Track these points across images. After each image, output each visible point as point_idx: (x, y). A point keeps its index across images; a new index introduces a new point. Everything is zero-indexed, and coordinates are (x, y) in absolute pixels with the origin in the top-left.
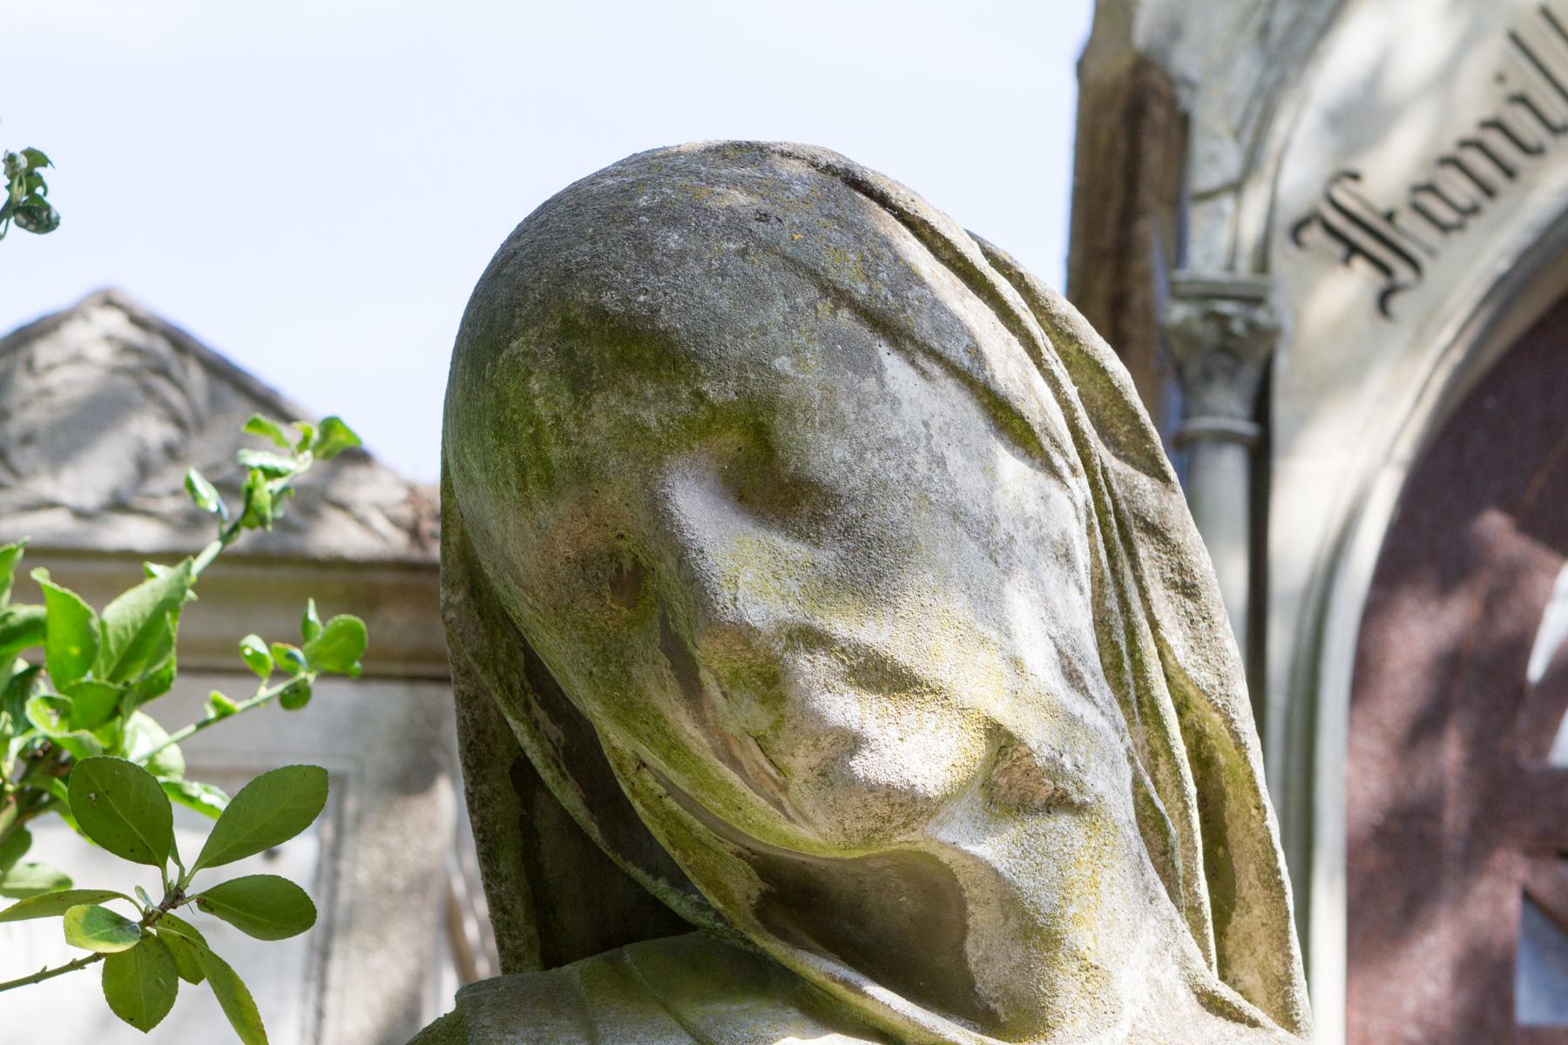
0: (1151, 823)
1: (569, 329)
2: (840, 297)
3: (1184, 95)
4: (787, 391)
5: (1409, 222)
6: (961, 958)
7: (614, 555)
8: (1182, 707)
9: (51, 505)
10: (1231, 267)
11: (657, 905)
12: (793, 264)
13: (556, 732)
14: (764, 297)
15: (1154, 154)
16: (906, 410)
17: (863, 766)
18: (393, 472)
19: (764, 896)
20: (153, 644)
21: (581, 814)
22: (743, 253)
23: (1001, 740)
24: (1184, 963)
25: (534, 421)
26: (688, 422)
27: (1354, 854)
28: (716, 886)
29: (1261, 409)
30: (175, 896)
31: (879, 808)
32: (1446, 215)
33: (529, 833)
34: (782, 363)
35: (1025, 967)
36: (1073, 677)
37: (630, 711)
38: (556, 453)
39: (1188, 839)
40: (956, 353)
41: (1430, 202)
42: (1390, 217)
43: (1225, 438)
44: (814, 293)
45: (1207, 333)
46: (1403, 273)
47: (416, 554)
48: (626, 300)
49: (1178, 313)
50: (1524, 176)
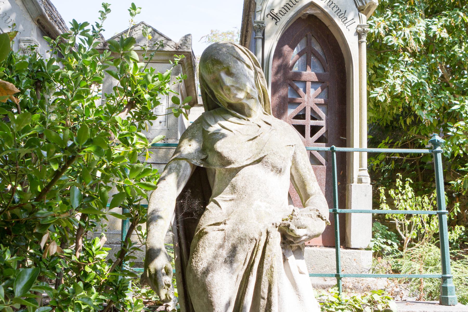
0: (259, 98)
1: (212, 60)
2: (234, 57)
5: (279, 14)
8: (262, 87)
9: (139, 45)
11: (217, 105)
12: (231, 54)
14: (228, 57)
15: (252, 6)
20: (168, 78)
21: (211, 98)
23: (248, 93)
29: (263, 35)
32: (283, 14)
33: (207, 99)
35: (250, 112)
36: (253, 87)
37: (217, 91)
38: (211, 71)
41: (281, 12)
42: (277, 14)
43: (260, 38)
45: (258, 27)
46: (278, 20)
49: (255, 25)
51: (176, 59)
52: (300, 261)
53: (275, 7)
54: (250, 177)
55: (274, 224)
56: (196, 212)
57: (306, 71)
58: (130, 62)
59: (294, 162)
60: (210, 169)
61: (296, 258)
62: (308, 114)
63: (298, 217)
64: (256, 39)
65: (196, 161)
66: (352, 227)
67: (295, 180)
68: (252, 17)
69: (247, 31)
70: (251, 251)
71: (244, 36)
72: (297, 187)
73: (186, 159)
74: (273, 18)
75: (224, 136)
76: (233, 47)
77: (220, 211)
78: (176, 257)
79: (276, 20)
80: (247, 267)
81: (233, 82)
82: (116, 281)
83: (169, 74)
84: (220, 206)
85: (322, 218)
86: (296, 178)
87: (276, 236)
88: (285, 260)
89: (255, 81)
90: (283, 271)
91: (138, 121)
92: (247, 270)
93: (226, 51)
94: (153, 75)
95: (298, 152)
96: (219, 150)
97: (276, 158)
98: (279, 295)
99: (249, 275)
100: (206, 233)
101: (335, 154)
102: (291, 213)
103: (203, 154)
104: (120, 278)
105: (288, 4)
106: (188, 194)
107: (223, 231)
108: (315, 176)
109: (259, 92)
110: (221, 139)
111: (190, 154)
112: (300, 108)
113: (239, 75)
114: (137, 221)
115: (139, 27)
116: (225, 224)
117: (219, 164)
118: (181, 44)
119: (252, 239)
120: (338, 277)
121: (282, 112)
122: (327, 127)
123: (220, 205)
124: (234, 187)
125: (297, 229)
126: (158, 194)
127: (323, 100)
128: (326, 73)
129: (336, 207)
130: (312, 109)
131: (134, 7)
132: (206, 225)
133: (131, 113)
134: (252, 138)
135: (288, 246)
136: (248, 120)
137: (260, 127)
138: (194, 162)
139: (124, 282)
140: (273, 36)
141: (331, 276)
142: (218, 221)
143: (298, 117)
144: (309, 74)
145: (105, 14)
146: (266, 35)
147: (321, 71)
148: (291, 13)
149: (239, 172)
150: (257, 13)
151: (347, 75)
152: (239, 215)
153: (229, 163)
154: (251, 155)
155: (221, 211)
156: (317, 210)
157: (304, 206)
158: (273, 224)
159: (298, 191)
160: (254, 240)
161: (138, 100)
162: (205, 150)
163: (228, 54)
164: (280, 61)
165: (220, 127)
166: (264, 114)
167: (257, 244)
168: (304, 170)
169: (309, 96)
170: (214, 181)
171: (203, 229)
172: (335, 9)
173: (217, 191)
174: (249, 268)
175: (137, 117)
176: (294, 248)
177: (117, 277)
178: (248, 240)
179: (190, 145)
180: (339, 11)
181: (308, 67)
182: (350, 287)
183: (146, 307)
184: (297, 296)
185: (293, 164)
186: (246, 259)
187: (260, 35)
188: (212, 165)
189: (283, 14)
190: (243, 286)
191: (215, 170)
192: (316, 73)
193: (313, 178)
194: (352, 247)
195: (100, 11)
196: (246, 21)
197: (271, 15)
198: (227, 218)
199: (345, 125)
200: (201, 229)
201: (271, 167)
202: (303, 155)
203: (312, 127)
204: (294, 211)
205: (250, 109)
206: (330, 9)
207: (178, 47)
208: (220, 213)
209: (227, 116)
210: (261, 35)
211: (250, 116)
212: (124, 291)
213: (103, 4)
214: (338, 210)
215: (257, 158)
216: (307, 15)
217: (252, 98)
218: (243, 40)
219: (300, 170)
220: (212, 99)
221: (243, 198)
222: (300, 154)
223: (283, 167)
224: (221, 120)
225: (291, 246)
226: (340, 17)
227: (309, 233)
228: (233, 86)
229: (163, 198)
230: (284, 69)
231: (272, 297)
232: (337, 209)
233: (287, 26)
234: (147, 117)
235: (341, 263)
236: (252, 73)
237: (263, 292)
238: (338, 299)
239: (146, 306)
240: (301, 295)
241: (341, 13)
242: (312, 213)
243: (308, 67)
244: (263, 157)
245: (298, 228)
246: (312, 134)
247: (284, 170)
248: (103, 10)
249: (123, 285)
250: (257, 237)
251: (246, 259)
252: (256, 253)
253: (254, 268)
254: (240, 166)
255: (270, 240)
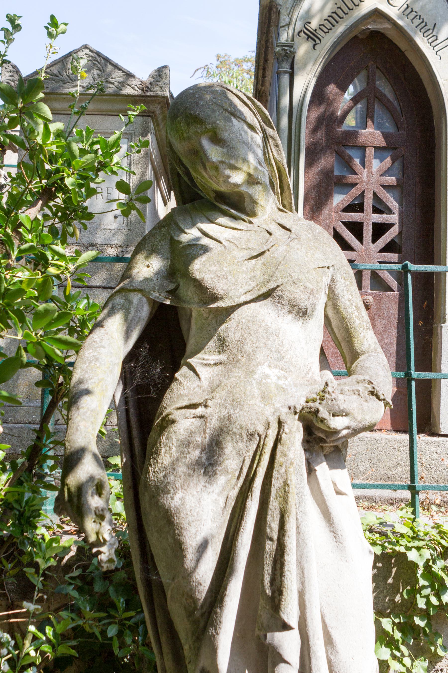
0: (271, 183)
1: (186, 117)
2: (226, 110)
3: (279, 7)
4: (219, 126)
6: (244, 205)
7: (194, 149)
8: (276, 163)
10: (287, 41)
12: (219, 106)
13: (184, 169)
14: (215, 112)
15: (274, 16)
16: (236, 127)
17: (231, 180)
18: (138, 79)
19: (216, 196)
20: (116, 145)
22: (212, 105)
23: (249, 175)
24: (276, 204)
25: (182, 130)
26: (204, 131)
27: (307, 149)
28: (209, 195)
29: (292, 67)
30: (131, 200)
31: (232, 186)
32: (326, 30)
33: (180, 183)
34: (218, 122)
35: (253, 207)
36: (260, 164)
38: (185, 135)
39: (277, 183)
40: (243, 117)
41: (322, 27)
42: (315, 30)
43: (286, 72)
44: (222, 110)
45: (283, 53)
46: (318, 41)
47: (143, 94)
48: (195, 113)
49: (278, 49)
50: (339, 23)
51: (130, 113)
52: (338, 472)
53: (312, 17)
54: (250, 325)
55: (292, 408)
56: (155, 385)
57: (365, 129)
58: (37, 124)
59: (331, 296)
60: (184, 309)
61: (331, 467)
62: (369, 203)
63: (334, 395)
64: (279, 73)
65: (158, 295)
66: (442, 397)
67: (334, 326)
68: (274, 35)
69: (266, 60)
70: (251, 455)
71: (261, 68)
72: (337, 338)
73: (140, 291)
74: (309, 37)
75: (205, 249)
76: (225, 92)
77: (198, 383)
78: (124, 460)
79: (315, 41)
80: (244, 483)
81: (224, 155)
82: (19, 502)
83: (118, 139)
84: (197, 375)
85: (378, 397)
86: (334, 323)
87: (294, 429)
88: (311, 471)
89: (264, 153)
90: (307, 489)
91: (61, 222)
92: (244, 487)
93: (211, 100)
94: (91, 141)
95: (338, 277)
96: (197, 276)
97: (298, 291)
98: (298, 533)
99: (247, 497)
100: (173, 422)
101: (409, 276)
102: (322, 388)
103: (171, 282)
104: (28, 495)
105: (335, 13)
106: (143, 352)
107: (202, 420)
108: (369, 321)
109: (272, 171)
110: (201, 255)
111: (146, 279)
112: (354, 192)
113: (235, 143)
114: (61, 393)
115: (80, 54)
116: (206, 406)
117: (196, 299)
118: (151, 84)
119: (252, 435)
120: (412, 489)
121: (324, 199)
122: (401, 226)
123: (199, 372)
124: (222, 342)
125: (332, 418)
126: (89, 354)
127: (394, 178)
128: (400, 132)
129: (410, 369)
130: (375, 194)
131: (54, 22)
132: (174, 407)
133: (50, 208)
134: (255, 254)
135: (316, 447)
136: (250, 222)
137: (270, 234)
138: (155, 295)
139: (34, 503)
140: (309, 67)
141: (402, 487)
142: (195, 401)
143: (350, 208)
144: (371, 133)
145: (12, 34)
146: (295, 67)
147: (390, 128)
148: (341, 29)
149: (232, 316)
150: (281, 29)
151: (436, 136)
152: (229, 392)
153: (215, 298)
154: (254, 284)
155: (199, 384)
156: (370, 382)
157: (349, 373)
158: (290, 408)
159: (339, 346)
160: (256, 436)
161: (60, 186)
162: (175, 273)
163: (214, 106)
164: (322, 109)
165: (199, 234)
166: (280, 210)
167: (262, 443)
168: (350, 310)
169: (370, 172)
170: (189, 329)
171: (167, 415)
172: (417, 21)
173: (193, 347)
174: (248, 484)
175: (60, 214)
176: (327, 450)
177: (22, 495)
178: (245, 436)
179: (148, 266)
180: (424, 24)
181: (370, 123)
182: (438, 502)
183: (81, 539)
184: (332, 534)
185: (329, 298)
186: (242, 468)
187: (286, 67)
188: (185, 302)
189: (326, 30)
190: (237, 516)
191: (191, 311)
192: (382, 133)
193: (365, 324)
194: (442, 433)
195: (2, 29)
196: (263, 42)
197: (305, 33)
198: (209, 397)
199: (433, 223)
200: (164, 414)
201: (288, 307)
202: (348, 283)
203: (374, 225)
204: (327, 384)
205: (254, 202)
206: (408, 21)
207: (145, 88)
208: (198, 386)
209: (212, 214)
210: (289, 67)
211: (254, 214)
212: (35, 518)
213: (7, 17)
214: (415, 374)
215: (264, 290)
216: (368, 32)
217: (258, 183)
218: (260, 74)
219: (342, 310)
220: (190, 184)
221: (237, 362)
222: (343, 281)
223: (309, 306)
224: (202, 222)
225: (322, 447)
226: (425, 35)
227: (353, 425)
228: (222, 162)
229: (97, 359)
230: (327, 126)
231: (286, 538)
232: (413, 372)
233: (332, 51)
234: (76, 215)
235: (418, 467)
236: (258, 138)
237: (271, 528)
238: (412, 529)
239: (79, 537)
240: (339, 533)
241: (427, 28)
242: (360, 387)
243: (370, 123)
244: (274, 289)
245: (334, 416)
246: (375, 238)
247: (312, 311)
248: (9, 26)
249: (32, 509)
250: (261, 429)
251: (242, 468)
252: (260, 459)
253: (255, 485)
254: (234, 304)
255: (284, 436)
